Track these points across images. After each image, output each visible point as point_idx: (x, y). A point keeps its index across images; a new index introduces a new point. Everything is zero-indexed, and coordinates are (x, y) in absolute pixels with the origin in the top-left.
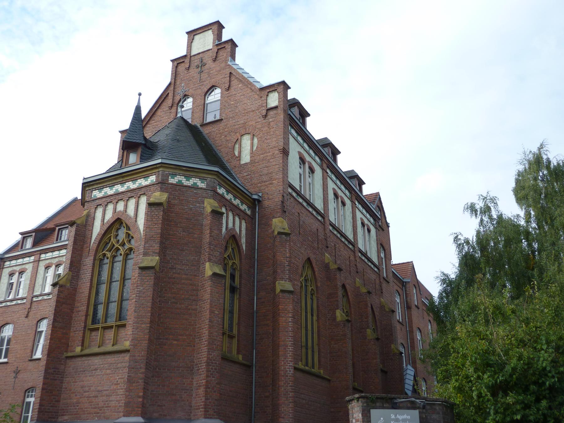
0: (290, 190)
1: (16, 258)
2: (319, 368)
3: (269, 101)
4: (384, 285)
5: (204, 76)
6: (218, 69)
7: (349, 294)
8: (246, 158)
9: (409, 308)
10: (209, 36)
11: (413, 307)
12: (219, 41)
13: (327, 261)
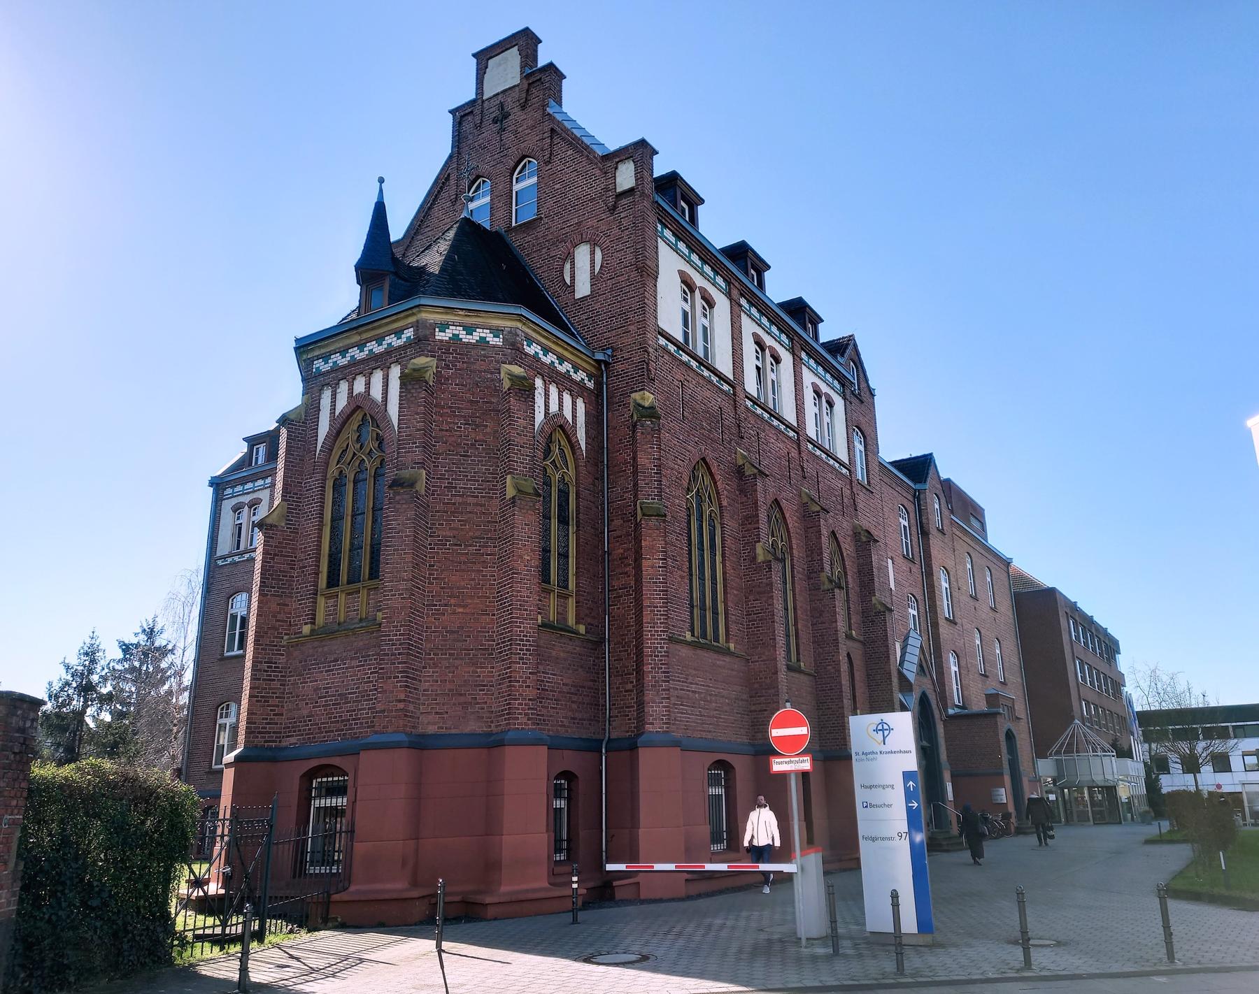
0: (662, 341)
1: (243, 481)
2: (727, 641)
3: (618, 180)
4: (861, 497)
5: (508, 137)
6: (530, 123)
7: (787, 516)
8: (583, 288)
9: (924, 533)
10: (513, 57)
11: (933, 531)
12: (531, 67)
13: (740, 462)
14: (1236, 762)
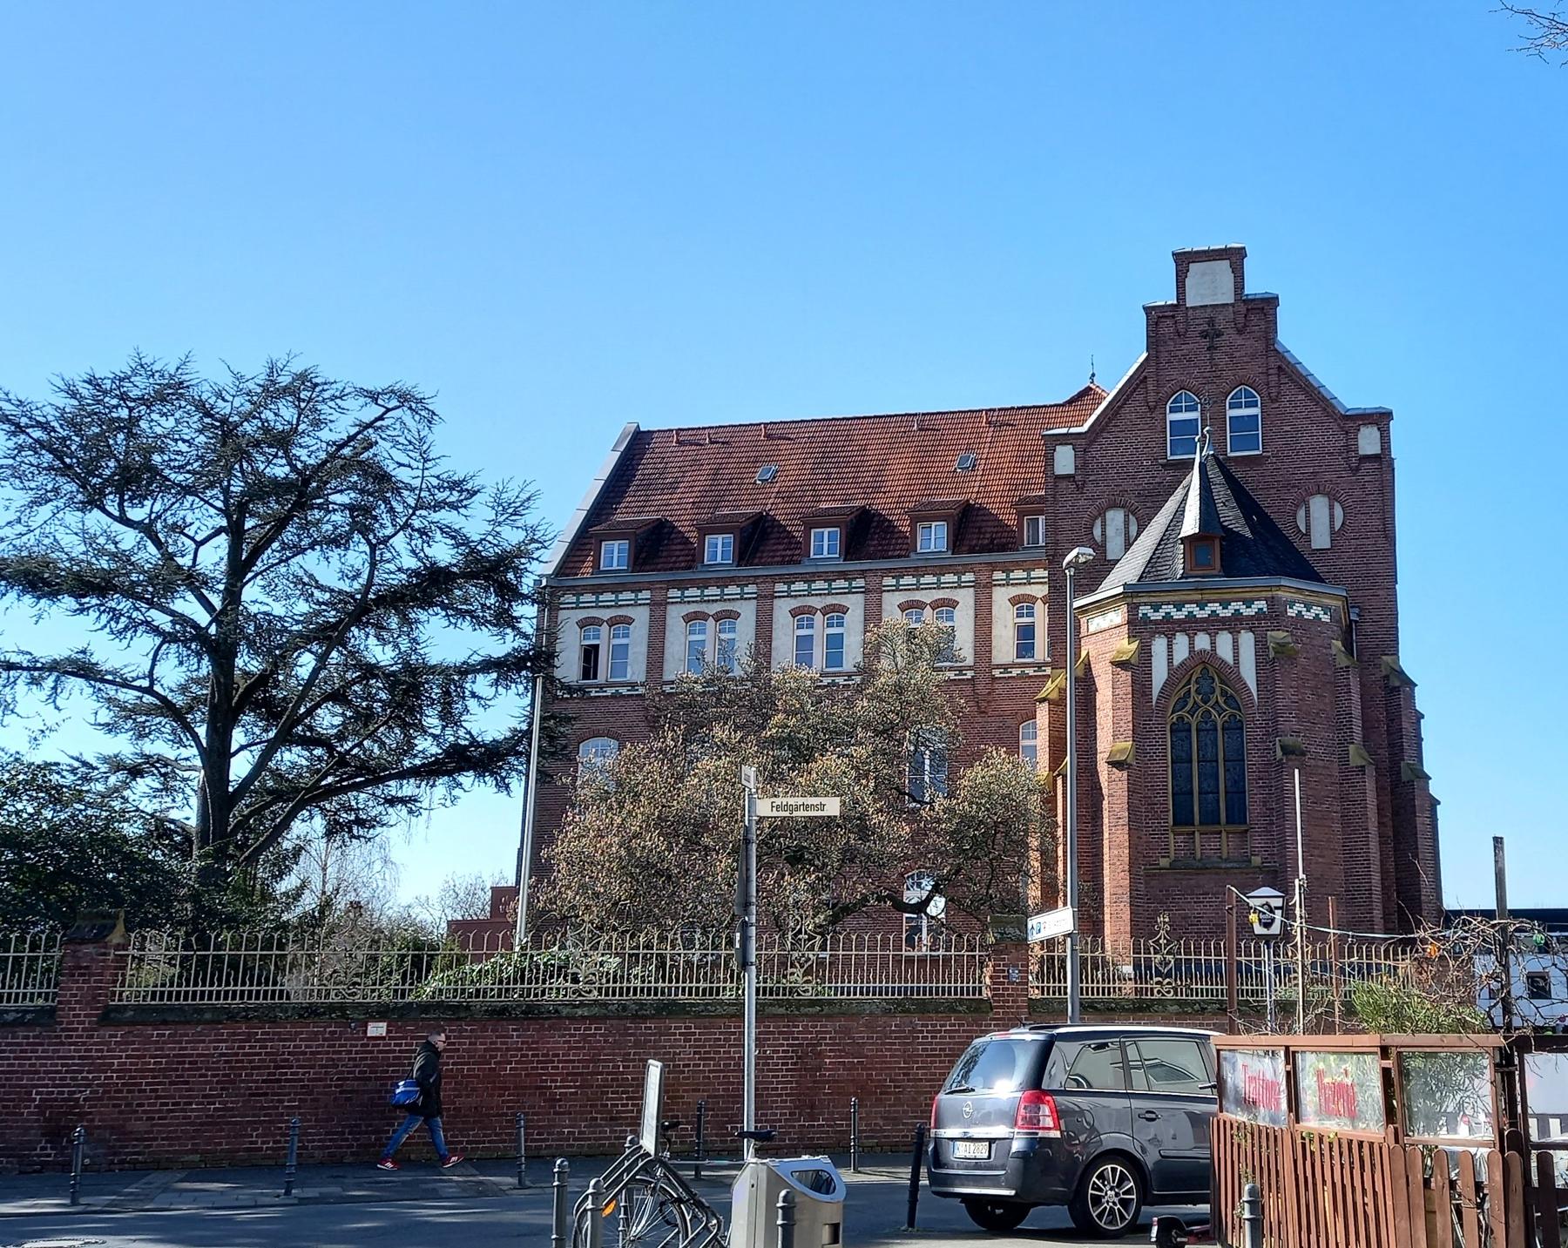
5: (1221, 359)
14: (1282, 992)
